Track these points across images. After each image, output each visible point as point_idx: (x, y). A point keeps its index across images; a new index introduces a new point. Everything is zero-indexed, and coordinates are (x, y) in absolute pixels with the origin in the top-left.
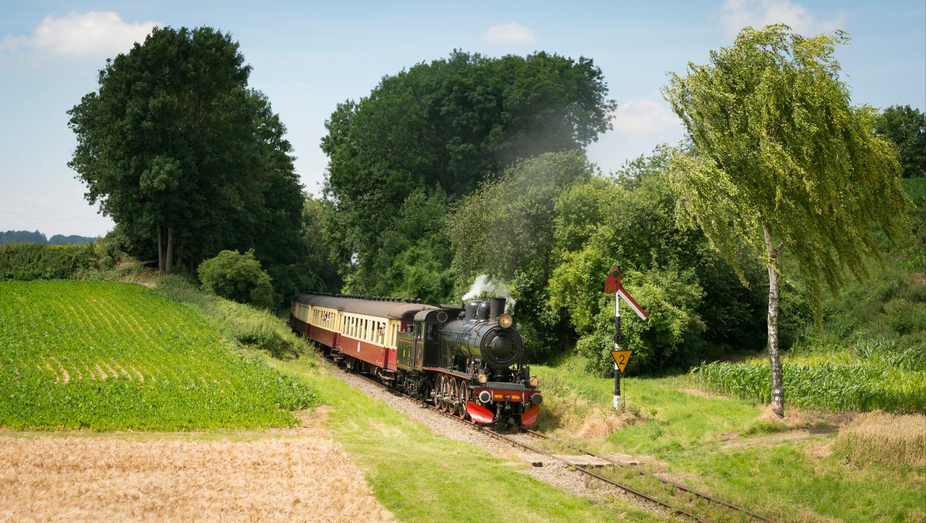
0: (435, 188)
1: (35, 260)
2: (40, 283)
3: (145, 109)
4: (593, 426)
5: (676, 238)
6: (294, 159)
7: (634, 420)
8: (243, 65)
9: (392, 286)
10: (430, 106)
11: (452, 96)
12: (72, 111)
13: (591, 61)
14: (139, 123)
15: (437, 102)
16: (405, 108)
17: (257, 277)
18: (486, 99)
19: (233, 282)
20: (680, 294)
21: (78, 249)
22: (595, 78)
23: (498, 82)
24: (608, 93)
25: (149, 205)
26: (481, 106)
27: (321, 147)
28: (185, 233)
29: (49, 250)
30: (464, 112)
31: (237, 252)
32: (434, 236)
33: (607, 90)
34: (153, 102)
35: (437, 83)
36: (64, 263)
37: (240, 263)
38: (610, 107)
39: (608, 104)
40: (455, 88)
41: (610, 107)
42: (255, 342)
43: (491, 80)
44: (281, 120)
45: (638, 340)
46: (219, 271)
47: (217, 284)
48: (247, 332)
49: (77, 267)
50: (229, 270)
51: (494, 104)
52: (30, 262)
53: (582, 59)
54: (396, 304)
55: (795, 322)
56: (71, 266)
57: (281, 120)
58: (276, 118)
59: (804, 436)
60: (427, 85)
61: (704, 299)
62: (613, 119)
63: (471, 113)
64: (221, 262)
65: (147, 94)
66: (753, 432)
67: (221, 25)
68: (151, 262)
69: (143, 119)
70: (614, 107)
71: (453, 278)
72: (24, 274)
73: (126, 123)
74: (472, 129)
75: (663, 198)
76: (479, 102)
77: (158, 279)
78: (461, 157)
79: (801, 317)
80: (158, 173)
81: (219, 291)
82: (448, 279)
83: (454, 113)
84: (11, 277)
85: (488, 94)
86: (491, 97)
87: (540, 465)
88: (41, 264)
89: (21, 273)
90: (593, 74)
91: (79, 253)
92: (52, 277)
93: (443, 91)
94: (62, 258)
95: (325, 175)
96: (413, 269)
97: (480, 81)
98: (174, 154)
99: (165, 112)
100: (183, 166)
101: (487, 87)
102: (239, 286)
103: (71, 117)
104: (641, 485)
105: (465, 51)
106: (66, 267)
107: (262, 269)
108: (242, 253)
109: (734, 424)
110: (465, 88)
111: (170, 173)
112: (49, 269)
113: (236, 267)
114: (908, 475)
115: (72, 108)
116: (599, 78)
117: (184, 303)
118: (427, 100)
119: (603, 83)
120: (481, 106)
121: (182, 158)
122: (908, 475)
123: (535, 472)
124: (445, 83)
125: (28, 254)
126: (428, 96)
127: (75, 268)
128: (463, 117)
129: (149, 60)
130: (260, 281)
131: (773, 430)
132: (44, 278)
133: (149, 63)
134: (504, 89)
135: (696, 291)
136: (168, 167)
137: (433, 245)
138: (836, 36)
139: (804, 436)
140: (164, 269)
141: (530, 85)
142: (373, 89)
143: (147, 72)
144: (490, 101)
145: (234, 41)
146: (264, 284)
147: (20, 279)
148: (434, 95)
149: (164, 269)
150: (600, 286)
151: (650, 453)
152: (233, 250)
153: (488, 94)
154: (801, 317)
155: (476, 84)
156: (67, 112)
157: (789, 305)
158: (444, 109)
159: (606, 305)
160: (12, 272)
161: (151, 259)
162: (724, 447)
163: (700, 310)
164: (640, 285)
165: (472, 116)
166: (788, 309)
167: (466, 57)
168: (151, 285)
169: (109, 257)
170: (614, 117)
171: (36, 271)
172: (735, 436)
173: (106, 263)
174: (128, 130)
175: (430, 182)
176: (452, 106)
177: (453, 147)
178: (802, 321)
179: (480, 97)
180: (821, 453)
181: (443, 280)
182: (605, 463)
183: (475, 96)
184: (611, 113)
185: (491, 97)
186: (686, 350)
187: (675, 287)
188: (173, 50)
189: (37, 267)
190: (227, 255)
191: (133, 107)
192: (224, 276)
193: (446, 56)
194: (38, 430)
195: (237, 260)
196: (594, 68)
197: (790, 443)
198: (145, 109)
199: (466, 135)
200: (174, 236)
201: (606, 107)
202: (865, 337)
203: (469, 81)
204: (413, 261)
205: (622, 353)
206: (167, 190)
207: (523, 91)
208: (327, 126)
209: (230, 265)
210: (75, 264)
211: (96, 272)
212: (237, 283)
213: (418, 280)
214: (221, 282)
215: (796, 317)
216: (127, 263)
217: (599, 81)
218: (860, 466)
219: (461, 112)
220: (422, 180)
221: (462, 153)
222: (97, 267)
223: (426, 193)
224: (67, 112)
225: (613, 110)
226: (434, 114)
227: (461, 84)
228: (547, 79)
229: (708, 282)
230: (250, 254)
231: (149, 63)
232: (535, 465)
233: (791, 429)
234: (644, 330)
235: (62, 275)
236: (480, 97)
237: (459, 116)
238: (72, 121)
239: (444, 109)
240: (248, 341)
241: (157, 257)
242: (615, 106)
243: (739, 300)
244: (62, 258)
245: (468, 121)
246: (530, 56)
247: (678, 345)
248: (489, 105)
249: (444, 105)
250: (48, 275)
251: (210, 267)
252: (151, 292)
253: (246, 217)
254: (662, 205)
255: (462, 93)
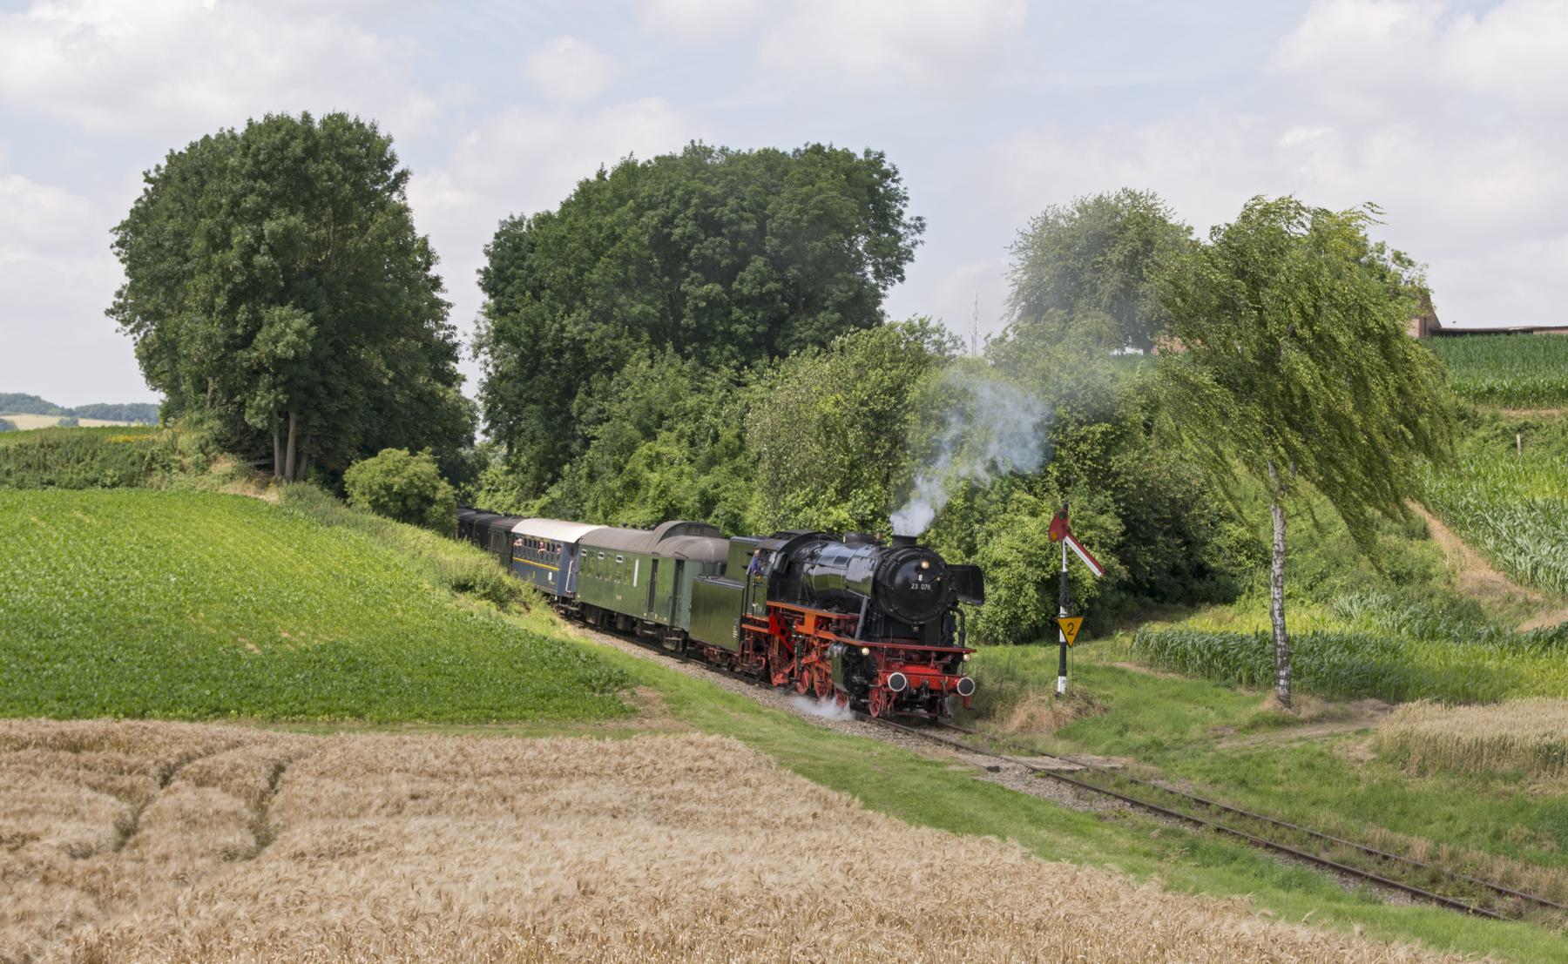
0: (663, 351)
1: (88, 459)
2: (97, 493)
3: (259, 238)
4: (1032, 717)
5: (1084, 447)
6: (449, 305)
7: (1086, 708)
8: (397, 169)
9: (622, 500)
10: (655, 228)
11: (690, 212)
12: (119, 229)
13: (882, 155)
14: (250, 258)
15: (668, 221)
16: (618, 230)
17: (435, 489)
18: (742, 218)
19: (402, 496)
20: (1091, 527)
21: (154, 442)
22: (889, 181)
23: (757, 193)
24: (908, 203)
25: (266, 379)
26: (734, 228)
27: (480, 284)
28: (316, 420)
29: (109, 443)
30: (707, 237)
31: (405, 452)
32: (681, 426)
33: (906, 198)
34: (269, 226)
35: (666, 194)
36: (133, 464)
37: (411, 469)
38: (915, 227)
39: (912, 223)
40: (695, 201)
41: (915, 227)
42: (471, 589)
43: (748, 191)
44: (432, 245)
45: (1031, 592)
46: (379, 479)
47: (377, 500)
48: (461, 574)
49: (152, 470)
50: (397, 479)
51: (753, 226)
52: (78, 462)
53: (868, 153)
54: (621, 530)
55: (1240, 564)
56: (144, 468)
57: (431, 245)
58: (425, 241)
59: (1321, 732)
60: (650, 196)
61: (1123, 534)
62: (919, 246)
63: (719, 239)
64: (385, 468)
65: (260, 215)
66: (1254, 726)
67: (358, 110)
68: (263, 462)
69: (256, 251)
70: (920, 226)
71: (719, 490)
72: (71, 479)
73: (233, 258)
74: (719, 262)
75: (1064, 392)
76: (731, 222)
77: (281, 490)
78: (704, 304)
79: (1249, 558)
80: (283, 333)
81: (378, 507)
82: (711, 491)
83: (693, 238)
84: (51, 483)
85: (743, 209)
86: (748, 215)
87: (996, 769)
88: (96, 465)
89: (66, 478)
90: (886, 175)
91: (155, 448)
92: (114, 485)
93: (675, 205)
94: (129, 456)
95: (476, 322)
96: (655, 477)
97: (731, 191)
98: (304, 303)
99: (285, 244)
100: (317, 321)
101: (743, 199)
102: (410, 502)
103: (117, 238)
104: (1139, 793)
105: (707, 144)
106: (136, 469)
107: (442, 476)
108: (413, 453)
109: (1225, 715)
110: (708, 201)
111: (300, 333)
112: (110, 472)
113: (405, 474)
114: (1492, 784)
115: (118, 224)
116: (893, 181)
117: (337, 528)
118: (652, 218)
119: (901, 188)
120: (734, 228)
121: (314, 309)
122: (1492, 784)
123: (992, 777)
124: (679, 193)
125: (76, 449)
126: (651, 213)
127: (150, 470)
128: (705, 243)
129: (263, 163)
130: (439, 495)
131: (1280, 723)
132: (104, 486)
133: (263, 167)
134: (768, 203)
135: (1112, 524)
136: (298, 323)
137: (678, 441)
138: (1363, 209)
139: (1321, 732)
140: (283, 472)
141: (809, 197)
142: (564, 200)
143: (260, 181)
144: (748, 221)
145: (382, 133)
146: (445, 499)
147: (66, 487)
148: (661, 211)
149: (283, 472)
150: (977, 515)
151: (1125, 754)
152: (400, 448)
153: (743, 209)
154: (1248, 558)
155: (726, 195)
156: (111, 231)
157: (1231, 542)
158: (678, 231)
159: (987, 543)
160: (53, 477)
161: (262, 458)
162: (1219, 746)
163: (1117, 550)
164: (1034, 514)
165: (721, 243)
166: (1230, 547)
167: (708, 152)
168: (272, 496)
169: (201, 455)
170: (922, 242)
171: (91, 475)
172: (1232, 732)
173: (196, 464)
174: (236, 268)
175: (657, 340)
176: (691, 227)
177: (691, 289)
178: (1250, 564)
179: (733, 216)
180: (1360, 755)
181: (703, 493)
182: (1078, 768)
183: (725, 213)
184: (917, 237)
185: (748, 215)
186: (1097, 606)
187: (1082, 519)
188: (297, 148)
189: (92, 469)
190: (392, 456)
191: (242, 235)
192: (388, 488)
193: (675, 147)
194: (294, 721)
195: (407, 463)
196: (886, 166)
197: (1310, 740)
198: (259, 238)
199: (710, 270)
200: (298, 423)
201: (909, 227)
202: (1347, 590)
203: (715, 190)
204: (654, 462)
205: (1070, 620)
206: (296, 359)
207: (797, 205)
208: (487, 253)
209: (398, 471)
210: (149, 464)
211: (182, 476)
212: (405, 498)
213: (663, 493)
214: (383, 496)
215: (1242, 558)
216: (226, 464)
217: (894, 185)
218: (1422, 772)
219: (702, 237)
220: (646, 336)
221: (706, 298)
222: (182, 469)
223: (651, 356)
224: (111, 231)
225: (919, 232)
226: (661, 241)
227: (704, 196)
228: (831, 190)
229: (1125, 509)
230: (425, 455)
231: (263, 167)
232: (990, 769)
233: (1303, 722)
234: (1043, 579)
235: (130, 481)
236: (733, 216)
237: (701, 242)
238: (118, 244)
239: (678, 231)
240: (463, 587)
241: (271, 455)
242: (922, 226)
243: (1165, 535)
244: (129, 456)
245: (714, 250)
246: (798, 150)
247: (1090, 600)
248: (745, 227)
249: (678, 226)
250: (108, 481)
251: (364, 473)
252: (272, 511)
253: (393, 394)
254: (1063, 402)
255: (706, 208)
